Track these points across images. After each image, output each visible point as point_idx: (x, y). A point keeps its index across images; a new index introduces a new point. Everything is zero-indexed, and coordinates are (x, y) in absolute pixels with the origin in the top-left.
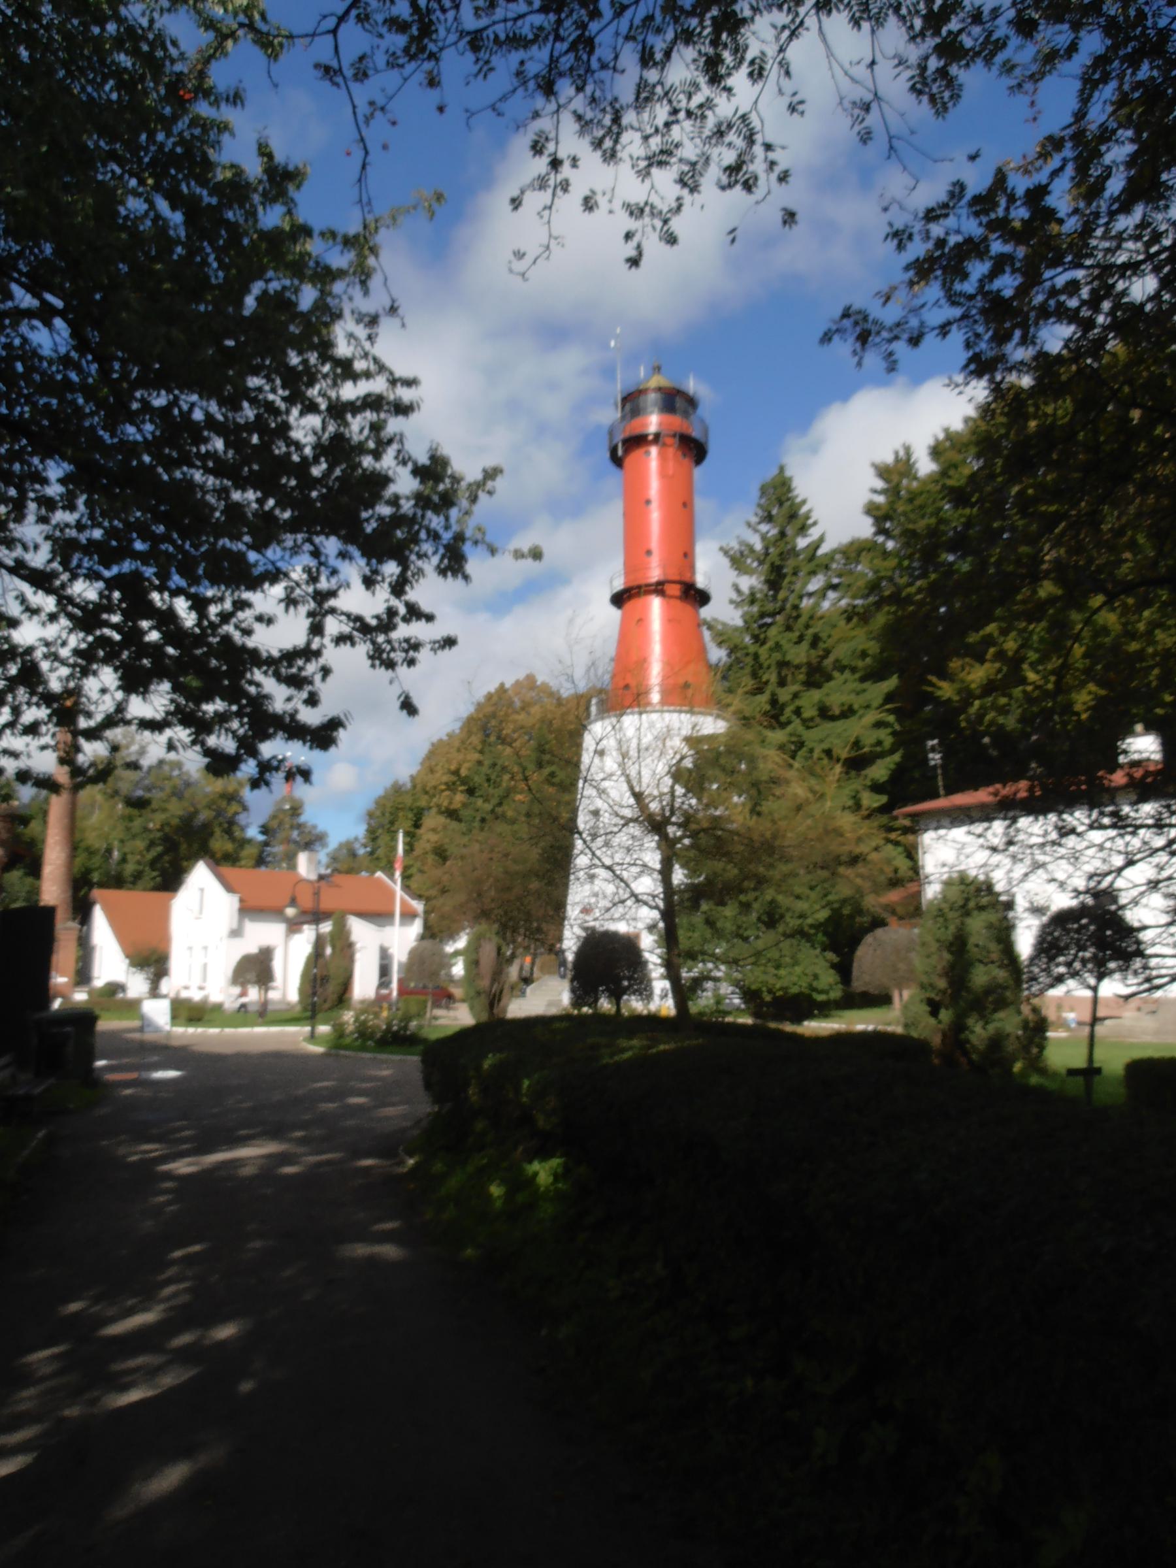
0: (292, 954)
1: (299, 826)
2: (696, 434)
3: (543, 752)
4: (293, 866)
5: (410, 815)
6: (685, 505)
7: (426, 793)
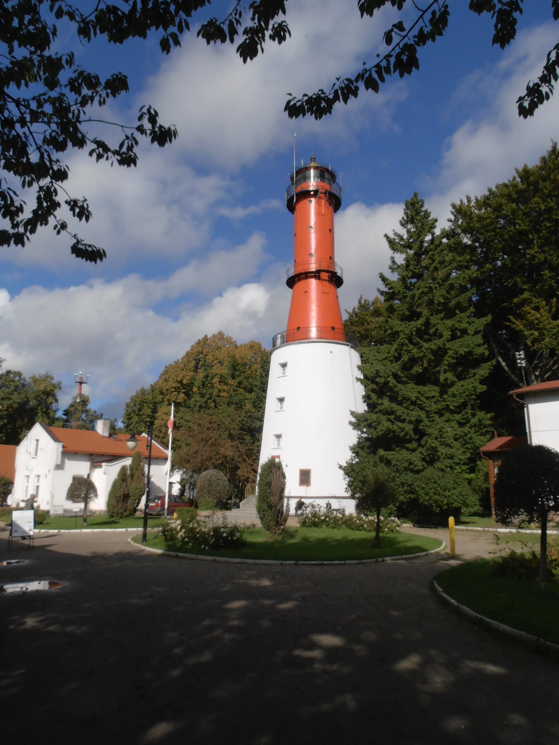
0: (104, 478)
1: (86, 411)
2: (336, 192)
3: (235, 370)
4: (93, 429)
5: (151, 406)
6: (330, 230)
7: (162, 393)
